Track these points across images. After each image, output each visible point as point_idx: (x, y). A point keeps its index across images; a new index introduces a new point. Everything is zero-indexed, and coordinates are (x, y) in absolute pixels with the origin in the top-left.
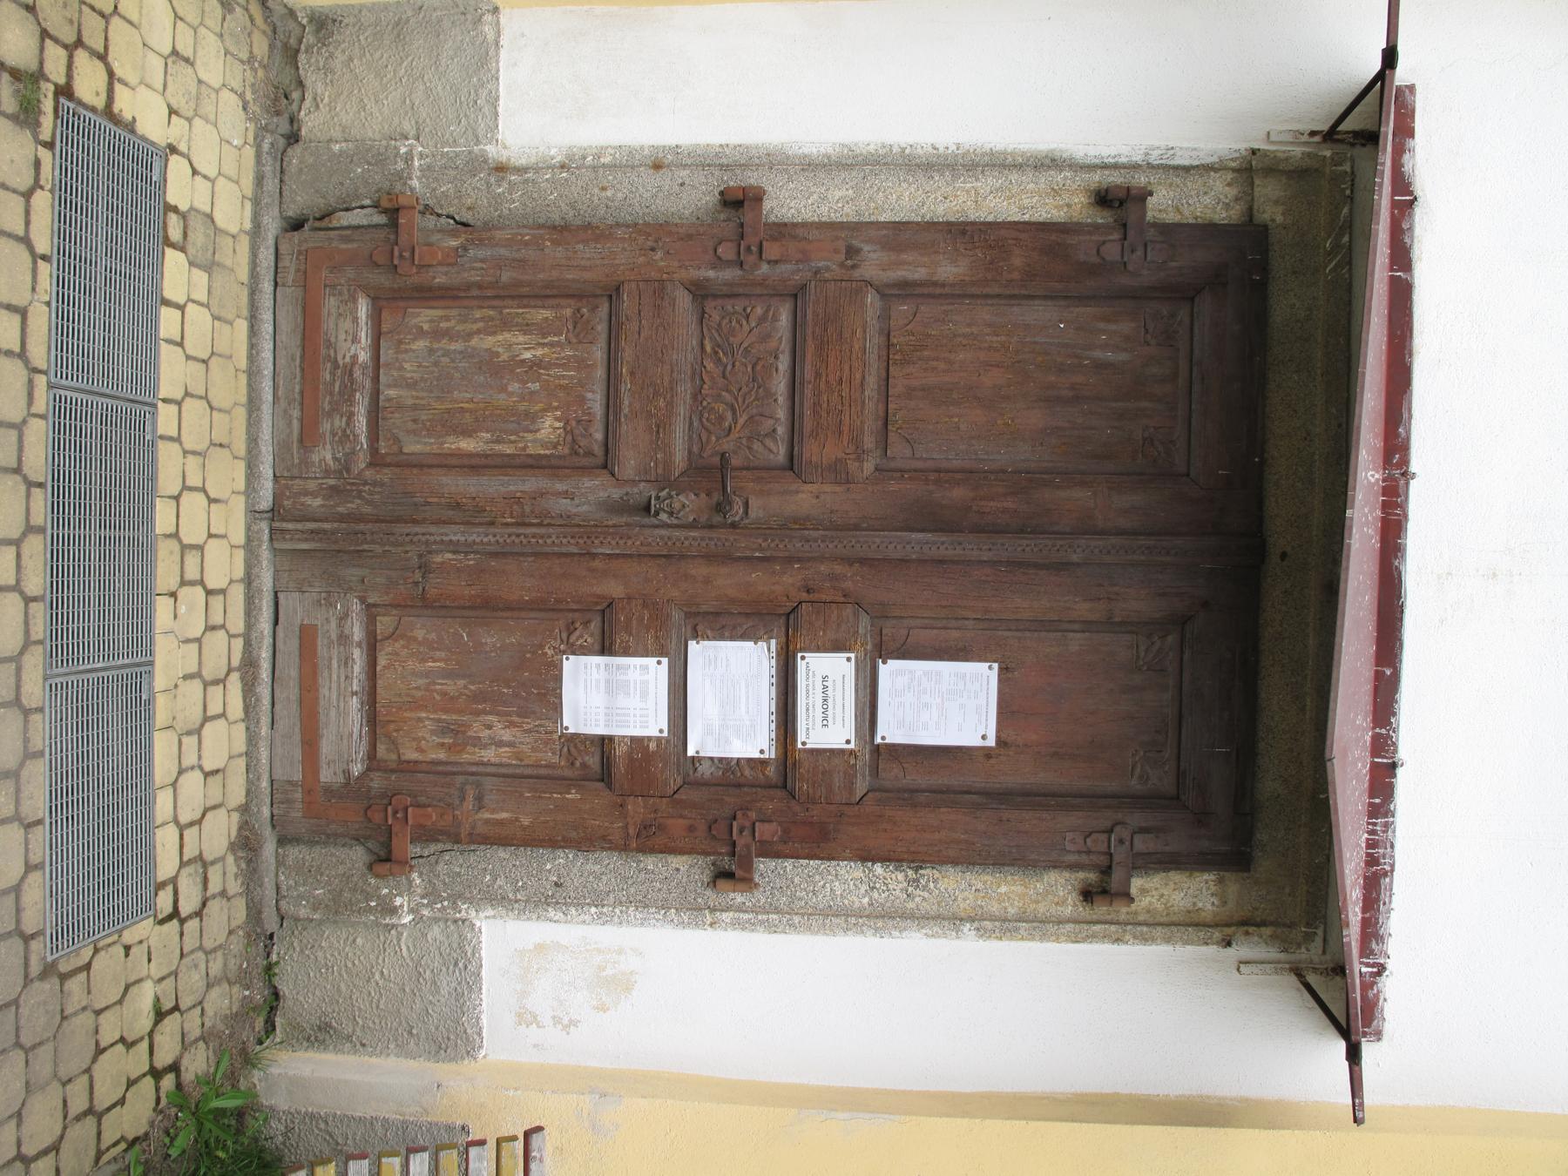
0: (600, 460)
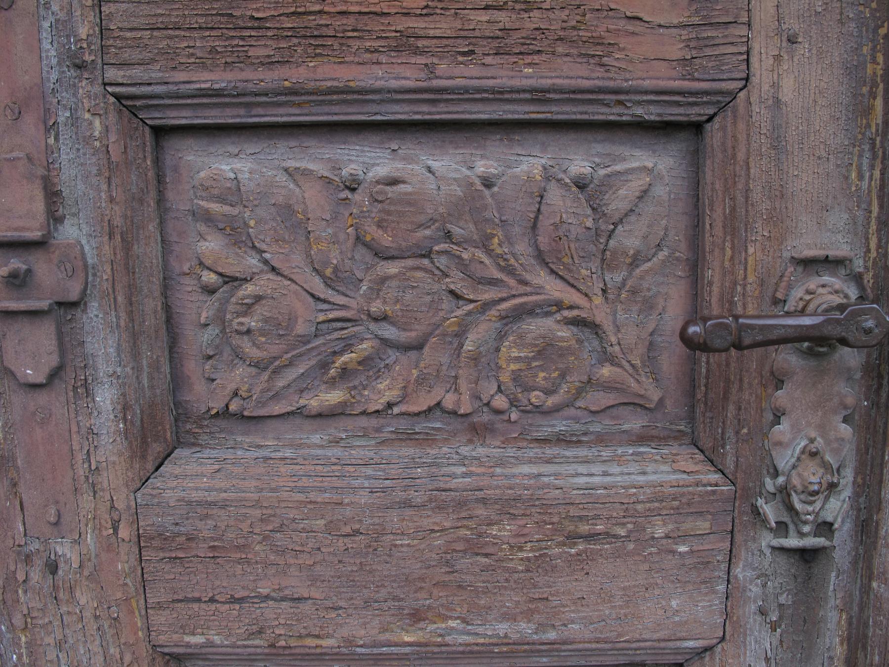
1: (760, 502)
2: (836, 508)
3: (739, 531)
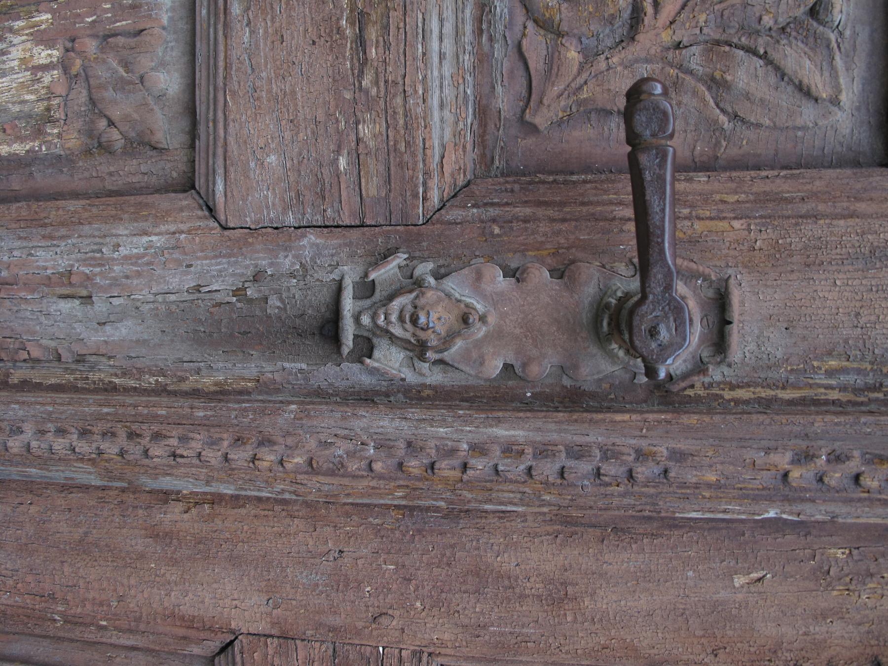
0: (172, 167)
1: (400, 258)
2: (390, 360)
3: (364, 234)
